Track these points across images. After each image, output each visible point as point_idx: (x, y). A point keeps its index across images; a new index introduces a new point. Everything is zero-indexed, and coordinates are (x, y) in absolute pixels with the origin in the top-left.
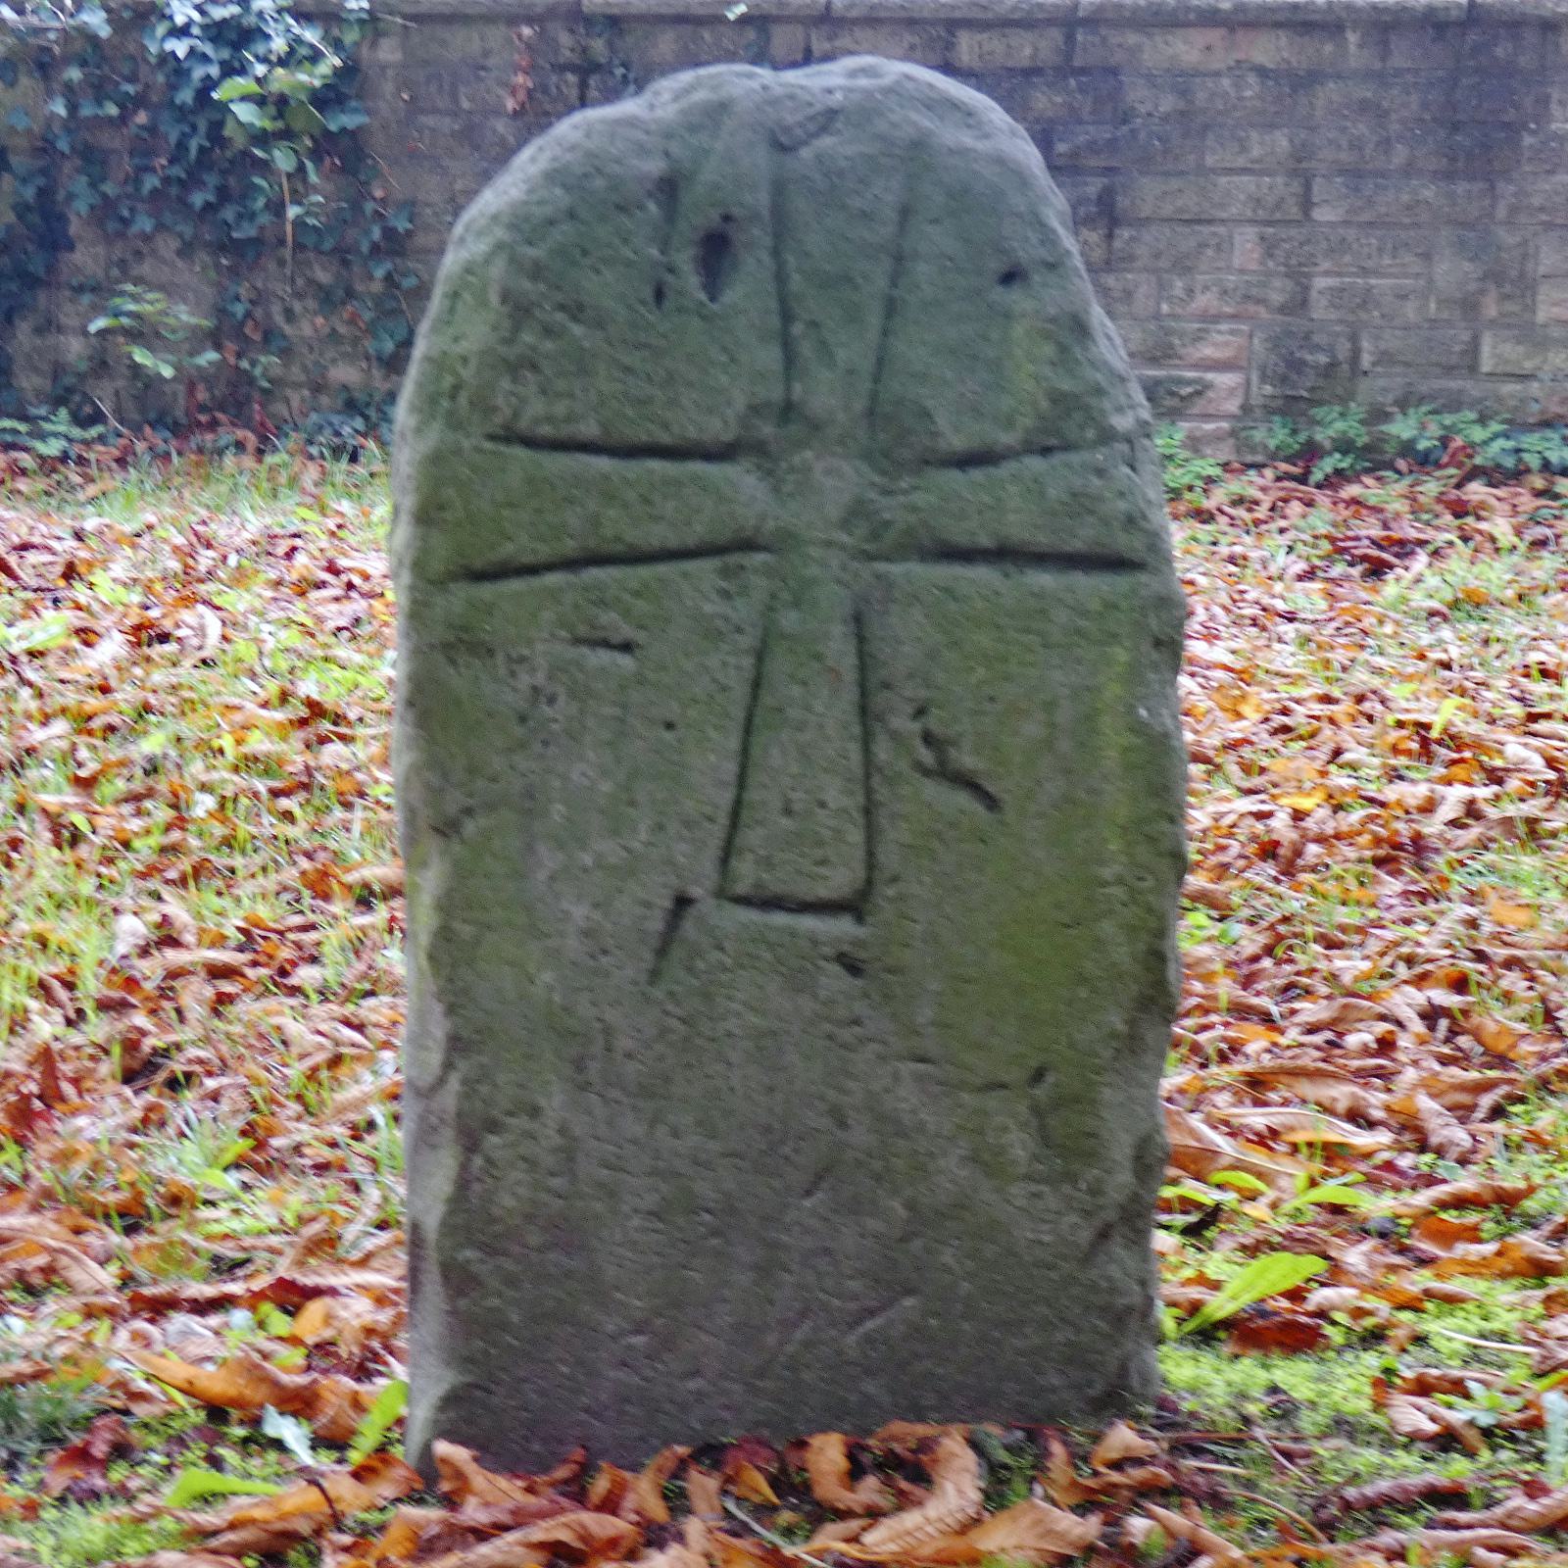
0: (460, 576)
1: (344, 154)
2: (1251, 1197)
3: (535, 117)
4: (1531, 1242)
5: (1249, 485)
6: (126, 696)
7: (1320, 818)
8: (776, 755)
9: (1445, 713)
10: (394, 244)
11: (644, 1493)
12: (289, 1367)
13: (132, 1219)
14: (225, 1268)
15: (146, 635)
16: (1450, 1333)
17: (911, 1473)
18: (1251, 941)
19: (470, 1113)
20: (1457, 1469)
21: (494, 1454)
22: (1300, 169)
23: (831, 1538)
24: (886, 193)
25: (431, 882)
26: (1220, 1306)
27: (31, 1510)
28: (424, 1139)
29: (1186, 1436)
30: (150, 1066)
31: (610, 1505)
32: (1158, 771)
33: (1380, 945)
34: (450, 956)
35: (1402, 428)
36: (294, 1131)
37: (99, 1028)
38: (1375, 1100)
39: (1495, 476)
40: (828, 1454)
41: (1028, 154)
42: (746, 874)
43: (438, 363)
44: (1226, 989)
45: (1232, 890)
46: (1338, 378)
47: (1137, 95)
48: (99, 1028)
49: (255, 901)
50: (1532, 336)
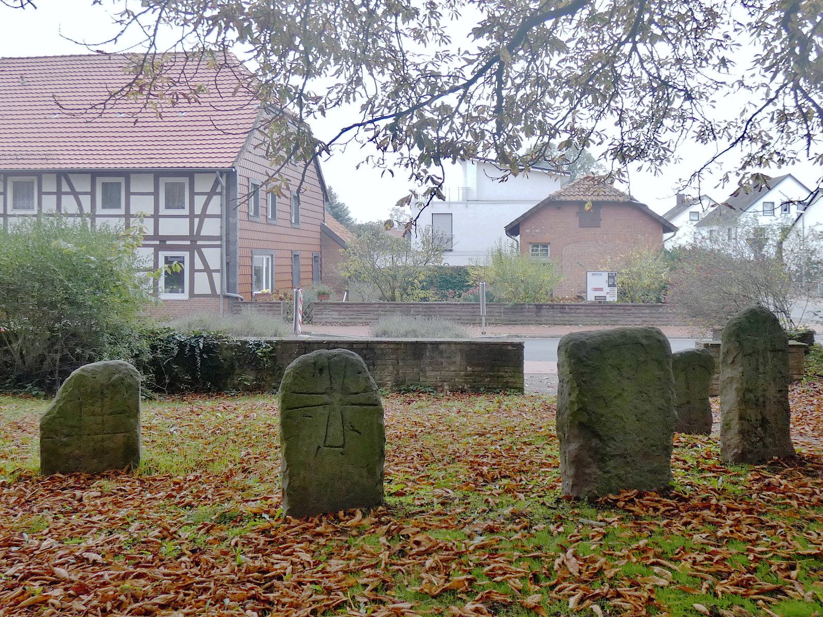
0: (288, 412)
1: (274, 359)
2: (396, 476)
3: (299, 354)
4: (431, 481)
5: (393, 394)
6: (243, 424)
7: (403, 432)
8: (331, 429)
9: (418, 420)
10: (280, 369)
11: (316, 520)
12: (266, 508)
13: (243, 490)
14: (256, 495)
15: (246, 416)
16: (422, 492)
17: (353, 515)
18: (395, 448)
19: (291, 472)
20: (423, 508)
21: (295, 517)
22: (397, 359)
23: (342, 524)
24: (343, 364)
25: (284, 446)
26: (392, 491)
27: (228, 529)
28: (284, 478)
29: (388, 507)
30: (246, 470)
31: (311, 522)
32: (381, 429)
33: (411, 448)
34: (287, 455)
35: (411, 388)
36: (266, 477)
37: (238, 466)
38: (411, 465)
39: (423, 393)
40: (341, 513)
41: (361, 359)
42: (328, 443)
43: (284, 384)
44: (392, 453)
45: (393, 441)
46: (403, 382)
47: (376, 351)
48: (238, 466)
49: (261, 449)
50: (426, 377)
